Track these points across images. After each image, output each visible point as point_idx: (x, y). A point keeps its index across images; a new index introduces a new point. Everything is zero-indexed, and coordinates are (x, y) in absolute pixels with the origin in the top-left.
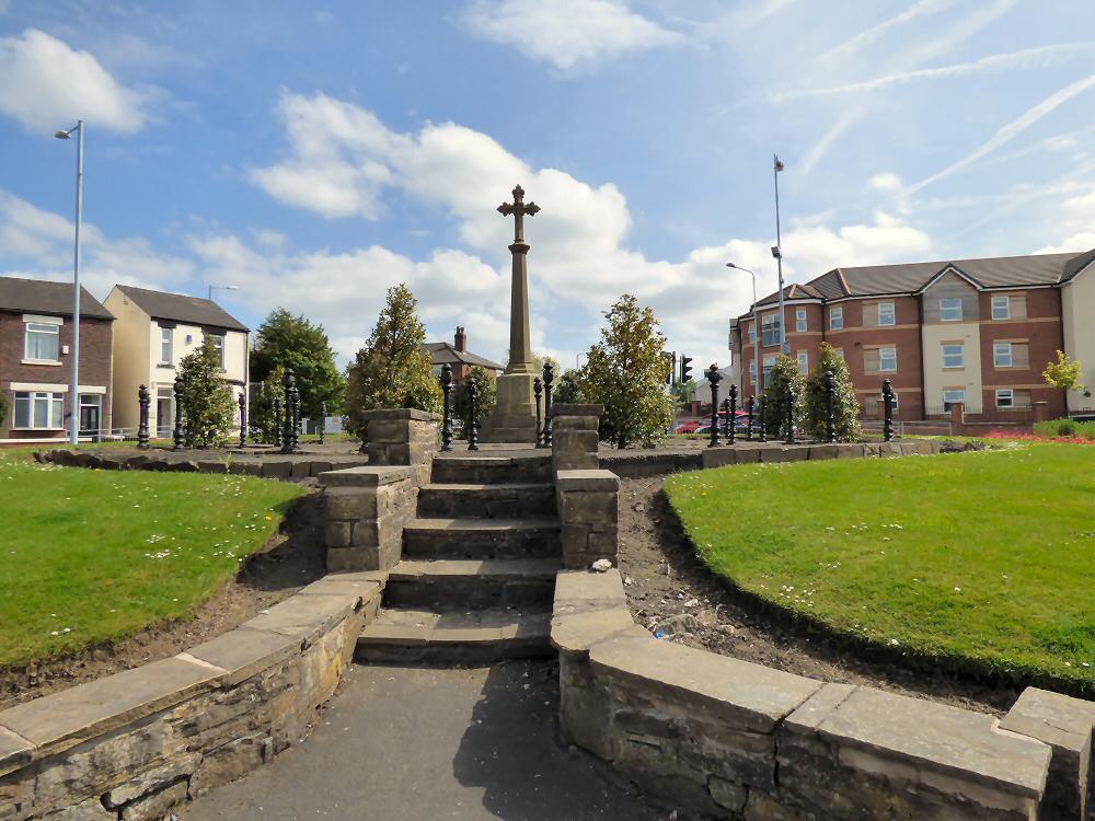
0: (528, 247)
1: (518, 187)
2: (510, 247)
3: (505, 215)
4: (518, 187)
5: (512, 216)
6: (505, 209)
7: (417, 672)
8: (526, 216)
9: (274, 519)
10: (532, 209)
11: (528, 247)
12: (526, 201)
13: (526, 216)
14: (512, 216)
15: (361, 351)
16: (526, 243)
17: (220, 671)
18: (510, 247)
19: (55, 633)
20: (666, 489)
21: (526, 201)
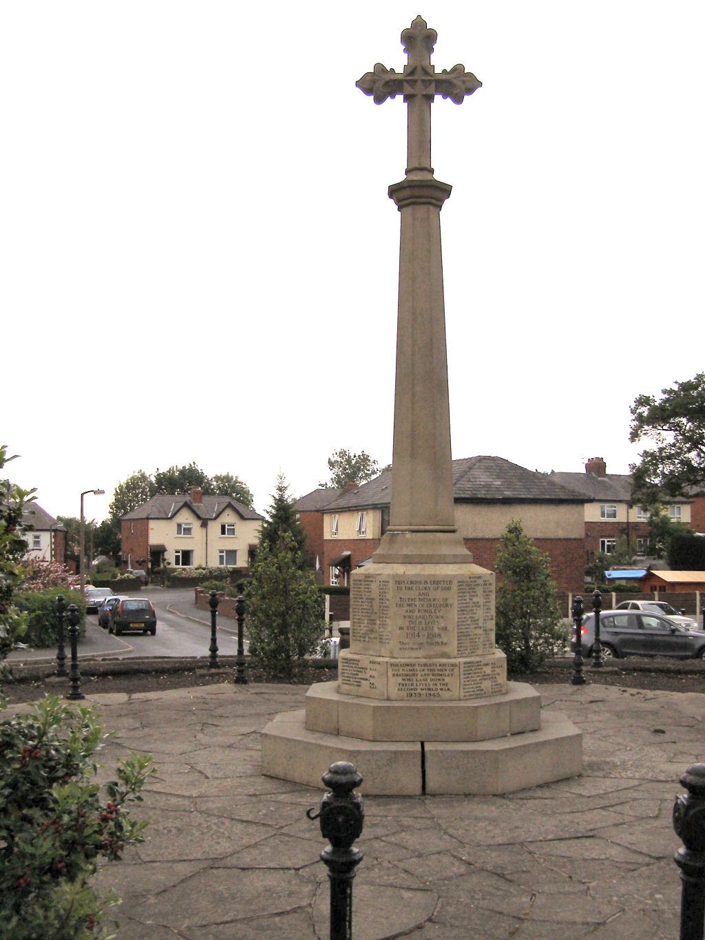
0: (446, 190)
1: (419, 23)
2: (394, 191)
3: (379, 100)
4: (419, 23)
5: (397, 106)
6: (378, 85)
7: (477, 566)
8: (441, 106)
9: (359, 453)
10: (459, 85)
11: (446, 190)
12: (441, 60)
13: (441, 106)
14: (397, 106)
15: (364, 459)
16: (440, 176)
17: (577, 790)
18: (394, 191)
19: (615, 881)
20: (505, 679)
21: (441, 60)
